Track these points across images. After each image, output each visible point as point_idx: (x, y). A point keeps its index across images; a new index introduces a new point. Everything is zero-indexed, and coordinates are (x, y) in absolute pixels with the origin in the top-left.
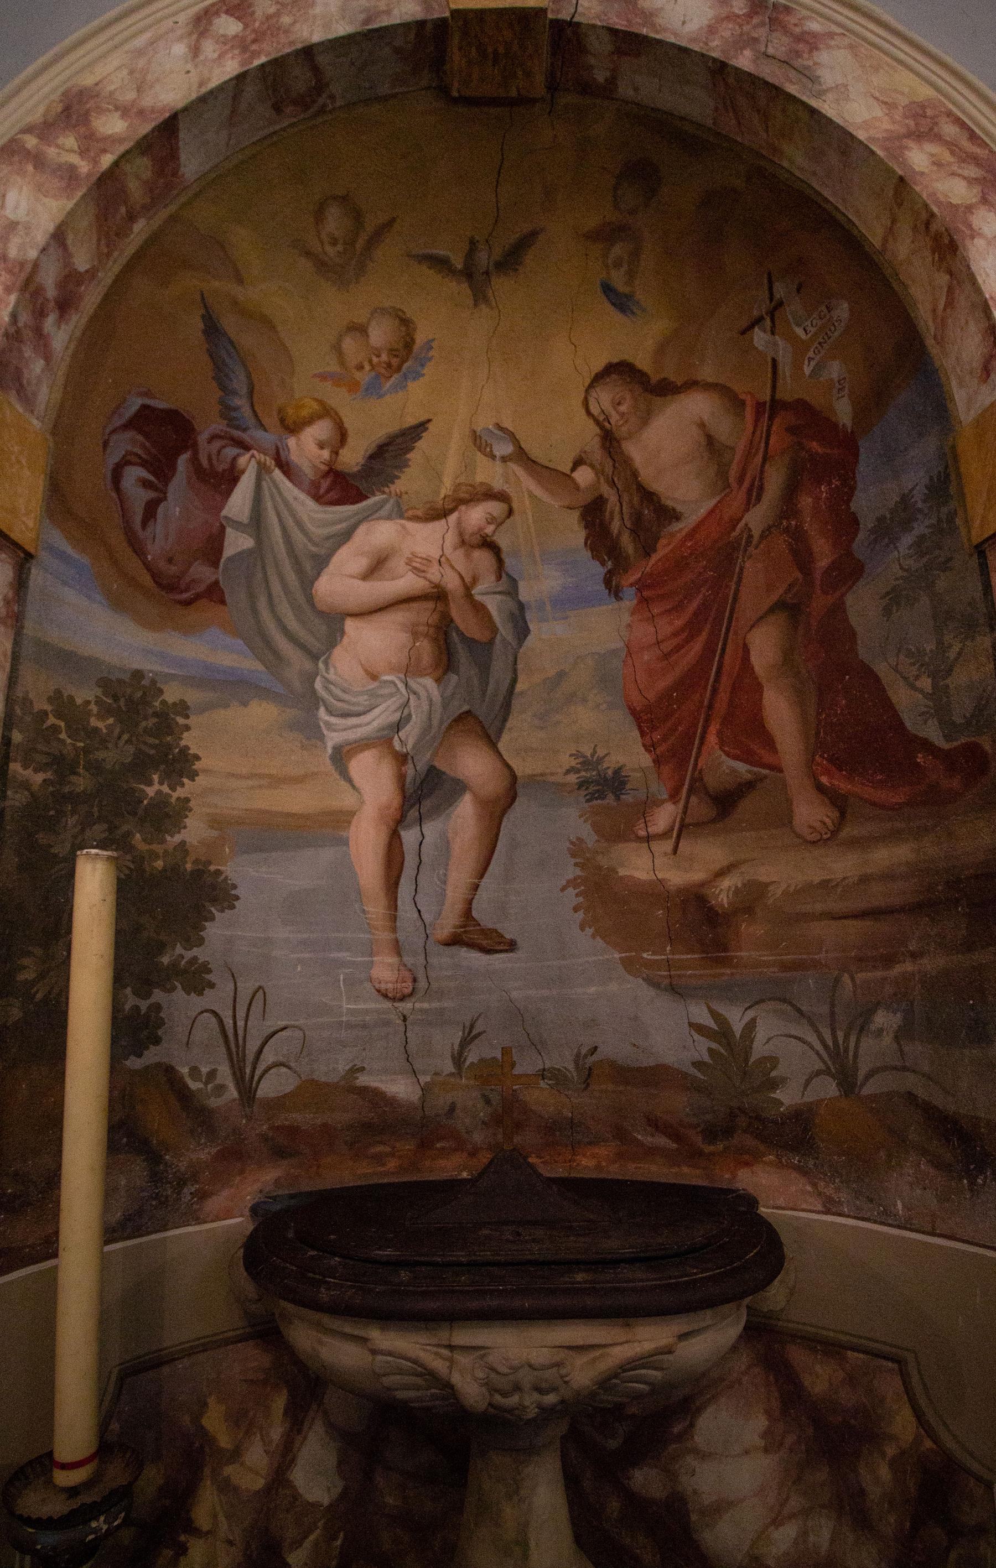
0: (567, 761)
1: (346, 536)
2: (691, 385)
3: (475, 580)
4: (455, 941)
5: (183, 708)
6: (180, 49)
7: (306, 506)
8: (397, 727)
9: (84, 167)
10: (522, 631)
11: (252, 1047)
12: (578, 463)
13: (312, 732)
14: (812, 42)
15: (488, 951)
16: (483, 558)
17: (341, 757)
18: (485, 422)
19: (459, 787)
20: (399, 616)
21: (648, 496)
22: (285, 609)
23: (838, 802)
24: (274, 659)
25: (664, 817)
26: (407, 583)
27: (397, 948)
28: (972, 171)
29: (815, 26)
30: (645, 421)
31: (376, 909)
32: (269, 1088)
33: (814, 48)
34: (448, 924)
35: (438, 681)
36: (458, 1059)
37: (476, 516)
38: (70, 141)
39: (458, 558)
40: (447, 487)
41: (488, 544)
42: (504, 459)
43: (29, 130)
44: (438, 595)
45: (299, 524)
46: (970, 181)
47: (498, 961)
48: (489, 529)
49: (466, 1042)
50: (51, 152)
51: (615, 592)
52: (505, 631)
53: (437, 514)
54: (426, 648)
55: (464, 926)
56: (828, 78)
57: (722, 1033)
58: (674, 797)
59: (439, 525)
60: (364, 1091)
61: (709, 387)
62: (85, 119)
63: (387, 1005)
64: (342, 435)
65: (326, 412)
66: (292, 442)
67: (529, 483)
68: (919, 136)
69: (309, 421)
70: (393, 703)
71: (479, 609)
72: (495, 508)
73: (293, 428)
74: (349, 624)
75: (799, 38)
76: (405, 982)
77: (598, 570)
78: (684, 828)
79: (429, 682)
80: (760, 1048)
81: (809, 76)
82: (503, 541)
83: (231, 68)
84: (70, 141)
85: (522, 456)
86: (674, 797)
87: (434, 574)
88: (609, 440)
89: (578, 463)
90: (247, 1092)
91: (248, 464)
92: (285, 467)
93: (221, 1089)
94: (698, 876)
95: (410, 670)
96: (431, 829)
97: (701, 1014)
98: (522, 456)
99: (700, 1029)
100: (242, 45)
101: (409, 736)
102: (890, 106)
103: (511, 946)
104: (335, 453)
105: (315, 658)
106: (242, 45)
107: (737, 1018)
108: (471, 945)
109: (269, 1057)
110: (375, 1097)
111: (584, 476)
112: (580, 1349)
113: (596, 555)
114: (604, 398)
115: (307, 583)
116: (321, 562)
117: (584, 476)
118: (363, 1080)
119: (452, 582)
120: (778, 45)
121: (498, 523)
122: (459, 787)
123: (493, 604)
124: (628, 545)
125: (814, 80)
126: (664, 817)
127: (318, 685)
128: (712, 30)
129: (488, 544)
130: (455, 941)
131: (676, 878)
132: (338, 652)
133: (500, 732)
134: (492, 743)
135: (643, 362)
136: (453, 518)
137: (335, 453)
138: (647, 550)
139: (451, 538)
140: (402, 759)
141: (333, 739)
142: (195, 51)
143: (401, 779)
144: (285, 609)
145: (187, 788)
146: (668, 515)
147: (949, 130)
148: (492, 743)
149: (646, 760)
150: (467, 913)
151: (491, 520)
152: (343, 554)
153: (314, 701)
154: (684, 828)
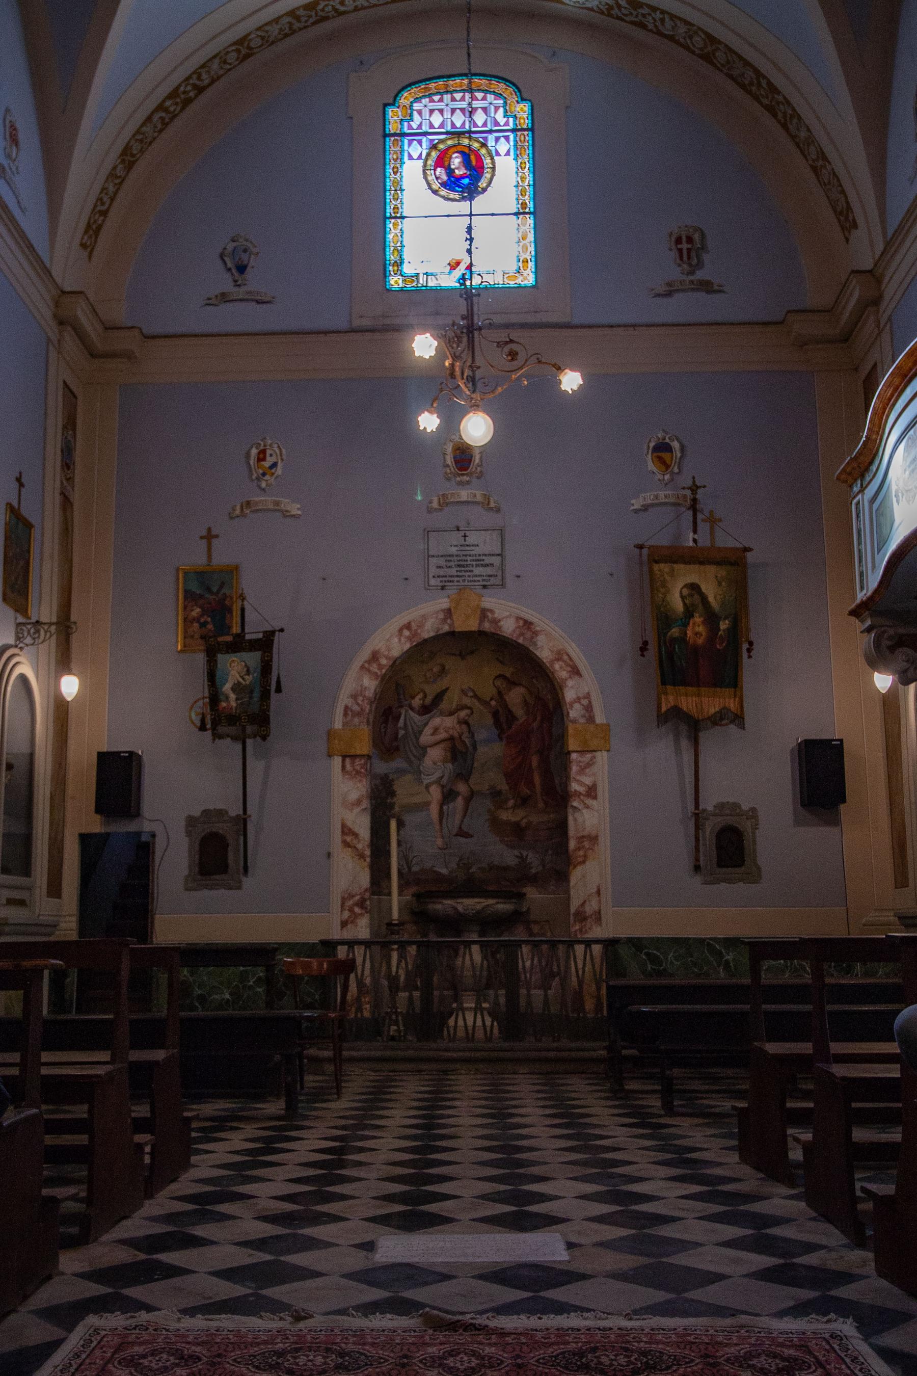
0: (487, 787)
1: (426, 724)
2: (520, 684)
3: (462, 733)
4: (457, 835)
5: (393, 780)
6: (396, 640)
7: (416, 717)
8: (442, 777)
9: (379, 673)
10: (475, 749)
11: (410, 860)
12: (491, 699)
13: (420, 781)
14: (536, 633)
15: (467, 838)
16: (464, 727)
17: (427, 787)
18: (465, 687)
19: (458, 794)
20: (442, 745)
21: (510, 711)
22: (412, 748)
23: (546, 803)
24: (410, 762)
25: (511, 803)
26: (443, 735)
27: (443, 837)
28: (569, 669)
29: (538, 628)
30: (510, 690)
31: (437, 827)
32: (415, 869)
33: (537, 635)
34: (455, 831)
35: (452, 764)
36: (458, 865)
37: (463, 714)
38: (375, 665)
39: (457, 726)
40: (454, 705)
41: (466, 723)
42: (471, 697)
43: (366, 662)
44: (451, 739)
45: (415, 723)
46: (568, 672)
47: (468, 840)
48: (466, 718)
49: (460, 861)
50: (371, 668)
51: (501, 739)
52: (471, 748)
53: (451, 714)
54: (449, 754)
55: (446, 1072)
56: (539, 644)
57: (521, 857)
58: (513, 798)
59: (453, 717)
60: (435, 872)
61: (524, 686)
62: (377, 660)
63: (440, 851)
64: (425, 696)
65: (422, 690)
66: (413, 701)
67: (477, 704)
68: (558, 660)
69: (417, 694)
70: (440, 771)
71: (463, 742)
72: (467, 711)
73: (413, 698)
74: (429, 749)
75: (534, 633)
76: (467, 835)
77: (496, 732)
78: (515, 807)
79: (450, 765)
80: (529, 860)
81: (535, 644)
82: (470, 721)
83: (408, 646)
84: (375, 665)
85: (476, 696)
86: (513, 798)
87: (451, 732)
88: (500, 693)
89: (491, 699)
90: (409, 868)
91: (403, 711)
92: (412, 709)
93: (404, 869)
94: (518, 819)
95: (444, 761)
96: (451, 805)
97: (516, 852)
98: (476, 696)
99: (517, 857)
100: (409, 639)
101: (445, 780)
102: (552, 652)
103: (472, 836)
104: (424, 701)
105: (419, 760)
106: (409, 639)
107: (525, 854)
108: (461, 836)
109: (414, 862)
110: (439, 874)
111: (493, 703)
112: (479, 903)
113: (496, 727)
114: (498, 683)
115: (417, 739)
116: (421, 732)
117: (493, 703)
118: (435, 869)
119: (456, 735)
120: (529, 635)
121: (469, 716)
122: (458, 794)
123: (467, 741)
124: (505, 726)
125: (536, 645)
126: (511, 803)
127: (421, 768)
128: (514, 631)
129: (466, 723)
130: (457, 835)
131: (513, 819)
132: (426, 758)
133: (469, 778)
134: (467, 781)
135: (508, 675)
136: (456, 715)
137: (424, 701)
138: (510, 728)
139: (455, 721)
140: (443, 787)
141: (425, 782)
142: (400, 640)
143: (443, 793)
144: (412, 748)
145: (395, 799)
146: (515, 718)
147: (565, 657)
148: (467, 781)
149: (507, 788)
150: (460, 828)
151: (467, 715)
152: (427, 728)
153: (420, 772)
154: (515, 807)
